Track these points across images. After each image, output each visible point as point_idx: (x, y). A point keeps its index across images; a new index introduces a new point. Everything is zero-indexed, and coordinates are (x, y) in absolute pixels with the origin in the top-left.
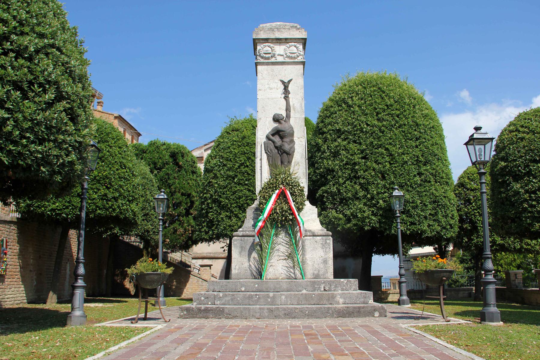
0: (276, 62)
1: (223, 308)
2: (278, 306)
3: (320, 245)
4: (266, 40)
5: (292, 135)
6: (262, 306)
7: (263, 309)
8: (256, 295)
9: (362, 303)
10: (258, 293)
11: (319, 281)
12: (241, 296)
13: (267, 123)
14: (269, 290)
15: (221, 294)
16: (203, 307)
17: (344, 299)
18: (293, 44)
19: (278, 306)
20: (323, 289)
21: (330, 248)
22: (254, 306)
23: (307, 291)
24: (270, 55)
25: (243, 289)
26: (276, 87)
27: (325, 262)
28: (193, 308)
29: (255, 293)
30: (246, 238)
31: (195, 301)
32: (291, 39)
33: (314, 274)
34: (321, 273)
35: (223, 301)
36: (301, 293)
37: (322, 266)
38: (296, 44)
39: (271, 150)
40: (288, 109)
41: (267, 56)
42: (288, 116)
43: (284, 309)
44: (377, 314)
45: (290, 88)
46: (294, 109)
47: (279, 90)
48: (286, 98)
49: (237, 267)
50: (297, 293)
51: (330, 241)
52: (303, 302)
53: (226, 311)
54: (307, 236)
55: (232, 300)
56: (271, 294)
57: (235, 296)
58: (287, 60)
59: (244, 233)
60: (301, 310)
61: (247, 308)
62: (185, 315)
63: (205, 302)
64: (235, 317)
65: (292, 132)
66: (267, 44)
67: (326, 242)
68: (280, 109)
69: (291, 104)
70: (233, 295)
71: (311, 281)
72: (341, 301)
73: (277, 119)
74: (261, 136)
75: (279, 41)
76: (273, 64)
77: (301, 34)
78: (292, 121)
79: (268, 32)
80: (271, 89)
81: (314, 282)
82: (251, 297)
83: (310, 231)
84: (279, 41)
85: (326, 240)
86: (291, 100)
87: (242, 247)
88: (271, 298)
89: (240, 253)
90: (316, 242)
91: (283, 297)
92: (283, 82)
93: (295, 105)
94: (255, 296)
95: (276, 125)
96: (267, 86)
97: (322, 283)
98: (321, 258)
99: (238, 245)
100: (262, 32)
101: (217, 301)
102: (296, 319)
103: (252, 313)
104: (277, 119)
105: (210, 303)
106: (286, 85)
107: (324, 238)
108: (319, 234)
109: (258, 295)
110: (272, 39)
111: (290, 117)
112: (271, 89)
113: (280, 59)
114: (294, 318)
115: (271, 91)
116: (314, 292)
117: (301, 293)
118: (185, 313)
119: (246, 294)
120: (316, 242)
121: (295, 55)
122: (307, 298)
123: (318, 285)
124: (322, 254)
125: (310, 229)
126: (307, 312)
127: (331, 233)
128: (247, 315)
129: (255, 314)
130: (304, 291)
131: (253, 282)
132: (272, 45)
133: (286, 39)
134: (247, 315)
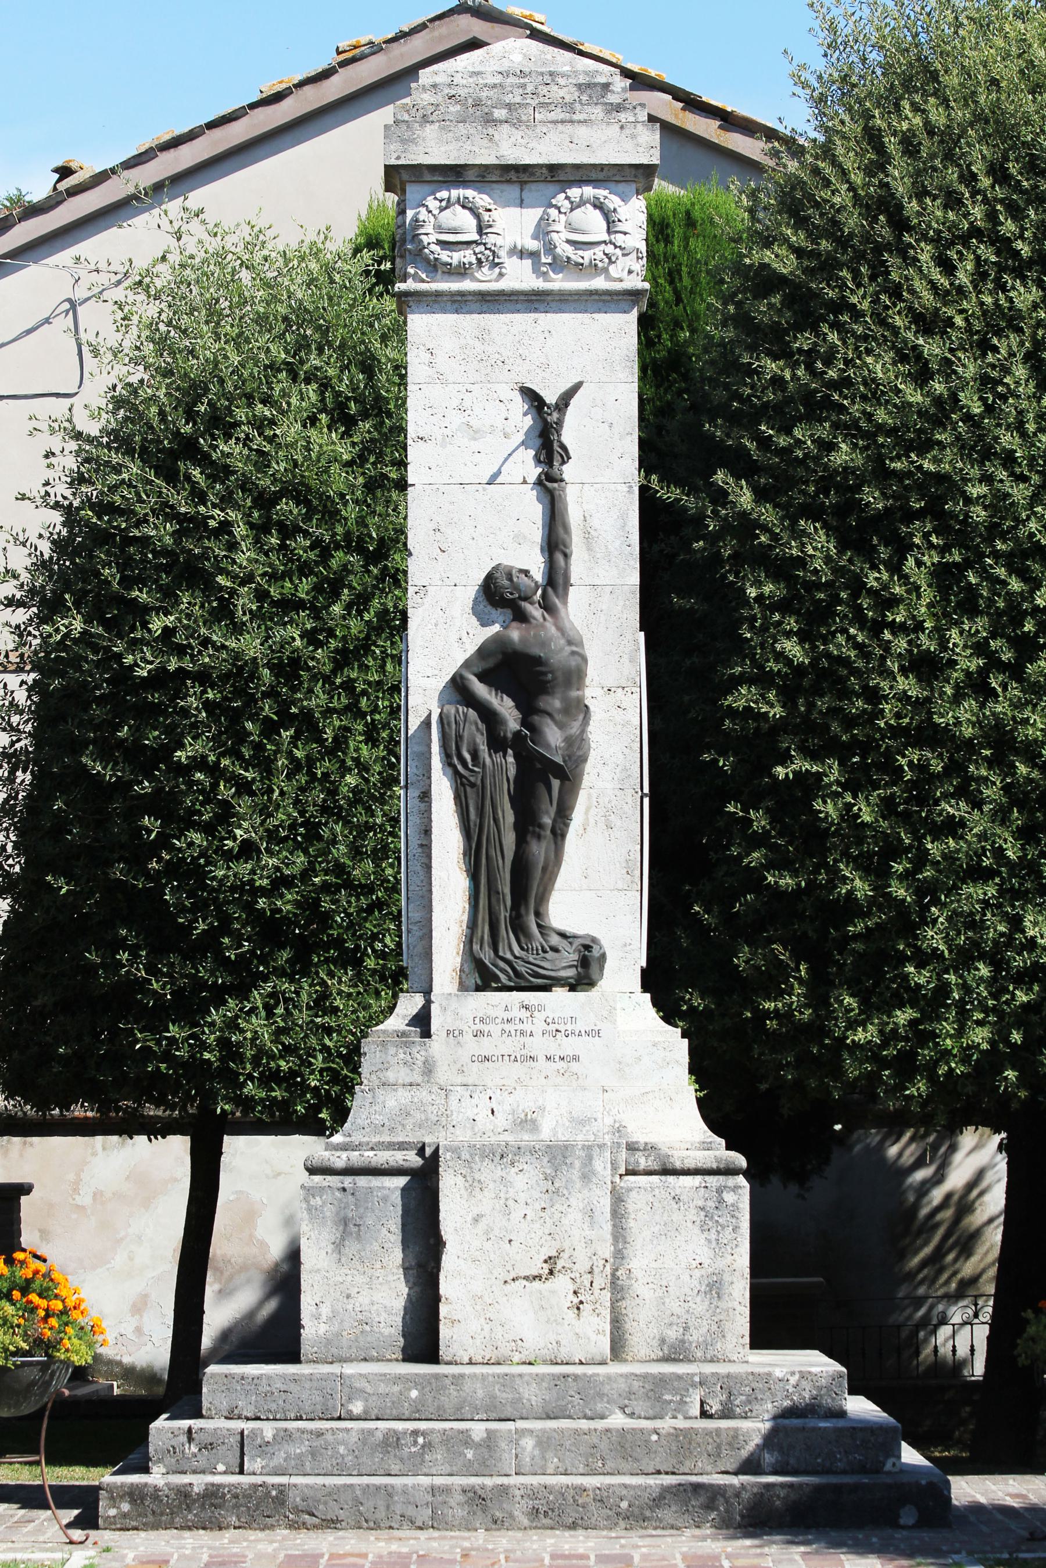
0: (501, 293)
1: (282, 1489)
2: (505, 1480)
3: (692, 1214)
4: (453, 174)
5: (575, 676)
6: (439, 1481)
7: (446, 1490)
8: (415, 1433)
9: (853, 1472)
10: (423, 1425)
11: (679, 1377)
12: (354, 1438)
14: (467, 1412)
15: (268, 1430)
16: (198, 1482)
17: (781, 1450)
18: (589, 191)
19: (505, 1480)
21: (735, 1229)
22: (409, 1481)
23: (632, 1415)
24: (467, 256)
25: (357, 1408)
27: (715, 1288)
28: (156, 1489)
29: (411, 1426)
30: (362, 1181)
31: (159, 1461)
33: (663, 1341)
34: (695, 1336)
35: (279, 1459)
36: (600, 1424)
37: (700, 1305)
38: (602, 193)
39: (475, 755)
40: (555, 544)
42: (556, 580)
43: (532, 1493)
44: (908, 1516)
45: (569, 435)
46: (588, 537)
48: (549, 486)
49: (325, 1310)
50: (584, 1424)
51: (739, 1193)
52: (610, 1465)
53: (295, 1498)
55: (313, 1453)
56: (478, 1430)
57: (329, 1437)
58: (559, 283)
59: (355, 1158)
60: (601, 1498)
61: (378, 1488)
62: (125, 1516)
63: (202, 1462)
64: (332, 1524)
65: (573, 662)
66: (455, 193)
67: (721, 1201)
68: (519, 539)
70: (319, 1434)
71: (645, 1377)
73: (498, 594)
74: (424, 690)
75: (517, 178)
77: (628, 145)
78: (577, 607)
81: (661, 1382)
82: (392, 1442)
83: (650, 1148)
84: (517, 178)
85: (720, 1191)
87: (345, 1222)
88: (477, 1446)
89: (339, 1246)
90: (676, 1199)
91: (528, 1444)
92: (532, 397)
93: (595, 522)
94: (409, 1440)
97: (693, 1385)
98: (697, 1273)
99: (329, 1211)
100: (430, 131)
101: (253, 1458)
102: (580, 1532)
103: (399, 1509)
104: (498, 594)
105: (221, 1468)
107: (713, 1181)
108: (690, 1164)
109: (424, 1434)
110: (486, 168)
111: (567, 584)
113: (519, 276)
114: (573, 1526)
115: (475, 446)
116: (658, 1424)
117: (600, 1424)
118: (126, 1507)
119: (371, 1432)
120: (676, 1199)
122: (626, 1447)
123: (675, 1391)
124: (704, 1254)
125: (651, 1139)
126: (624, 1505)
127: (742, 1161)
128: (381, 1514)
129: (410, 1511)
130: (617, 1420)
131: (398, 1379)
132: (482, 200)
134: (381, 1514)
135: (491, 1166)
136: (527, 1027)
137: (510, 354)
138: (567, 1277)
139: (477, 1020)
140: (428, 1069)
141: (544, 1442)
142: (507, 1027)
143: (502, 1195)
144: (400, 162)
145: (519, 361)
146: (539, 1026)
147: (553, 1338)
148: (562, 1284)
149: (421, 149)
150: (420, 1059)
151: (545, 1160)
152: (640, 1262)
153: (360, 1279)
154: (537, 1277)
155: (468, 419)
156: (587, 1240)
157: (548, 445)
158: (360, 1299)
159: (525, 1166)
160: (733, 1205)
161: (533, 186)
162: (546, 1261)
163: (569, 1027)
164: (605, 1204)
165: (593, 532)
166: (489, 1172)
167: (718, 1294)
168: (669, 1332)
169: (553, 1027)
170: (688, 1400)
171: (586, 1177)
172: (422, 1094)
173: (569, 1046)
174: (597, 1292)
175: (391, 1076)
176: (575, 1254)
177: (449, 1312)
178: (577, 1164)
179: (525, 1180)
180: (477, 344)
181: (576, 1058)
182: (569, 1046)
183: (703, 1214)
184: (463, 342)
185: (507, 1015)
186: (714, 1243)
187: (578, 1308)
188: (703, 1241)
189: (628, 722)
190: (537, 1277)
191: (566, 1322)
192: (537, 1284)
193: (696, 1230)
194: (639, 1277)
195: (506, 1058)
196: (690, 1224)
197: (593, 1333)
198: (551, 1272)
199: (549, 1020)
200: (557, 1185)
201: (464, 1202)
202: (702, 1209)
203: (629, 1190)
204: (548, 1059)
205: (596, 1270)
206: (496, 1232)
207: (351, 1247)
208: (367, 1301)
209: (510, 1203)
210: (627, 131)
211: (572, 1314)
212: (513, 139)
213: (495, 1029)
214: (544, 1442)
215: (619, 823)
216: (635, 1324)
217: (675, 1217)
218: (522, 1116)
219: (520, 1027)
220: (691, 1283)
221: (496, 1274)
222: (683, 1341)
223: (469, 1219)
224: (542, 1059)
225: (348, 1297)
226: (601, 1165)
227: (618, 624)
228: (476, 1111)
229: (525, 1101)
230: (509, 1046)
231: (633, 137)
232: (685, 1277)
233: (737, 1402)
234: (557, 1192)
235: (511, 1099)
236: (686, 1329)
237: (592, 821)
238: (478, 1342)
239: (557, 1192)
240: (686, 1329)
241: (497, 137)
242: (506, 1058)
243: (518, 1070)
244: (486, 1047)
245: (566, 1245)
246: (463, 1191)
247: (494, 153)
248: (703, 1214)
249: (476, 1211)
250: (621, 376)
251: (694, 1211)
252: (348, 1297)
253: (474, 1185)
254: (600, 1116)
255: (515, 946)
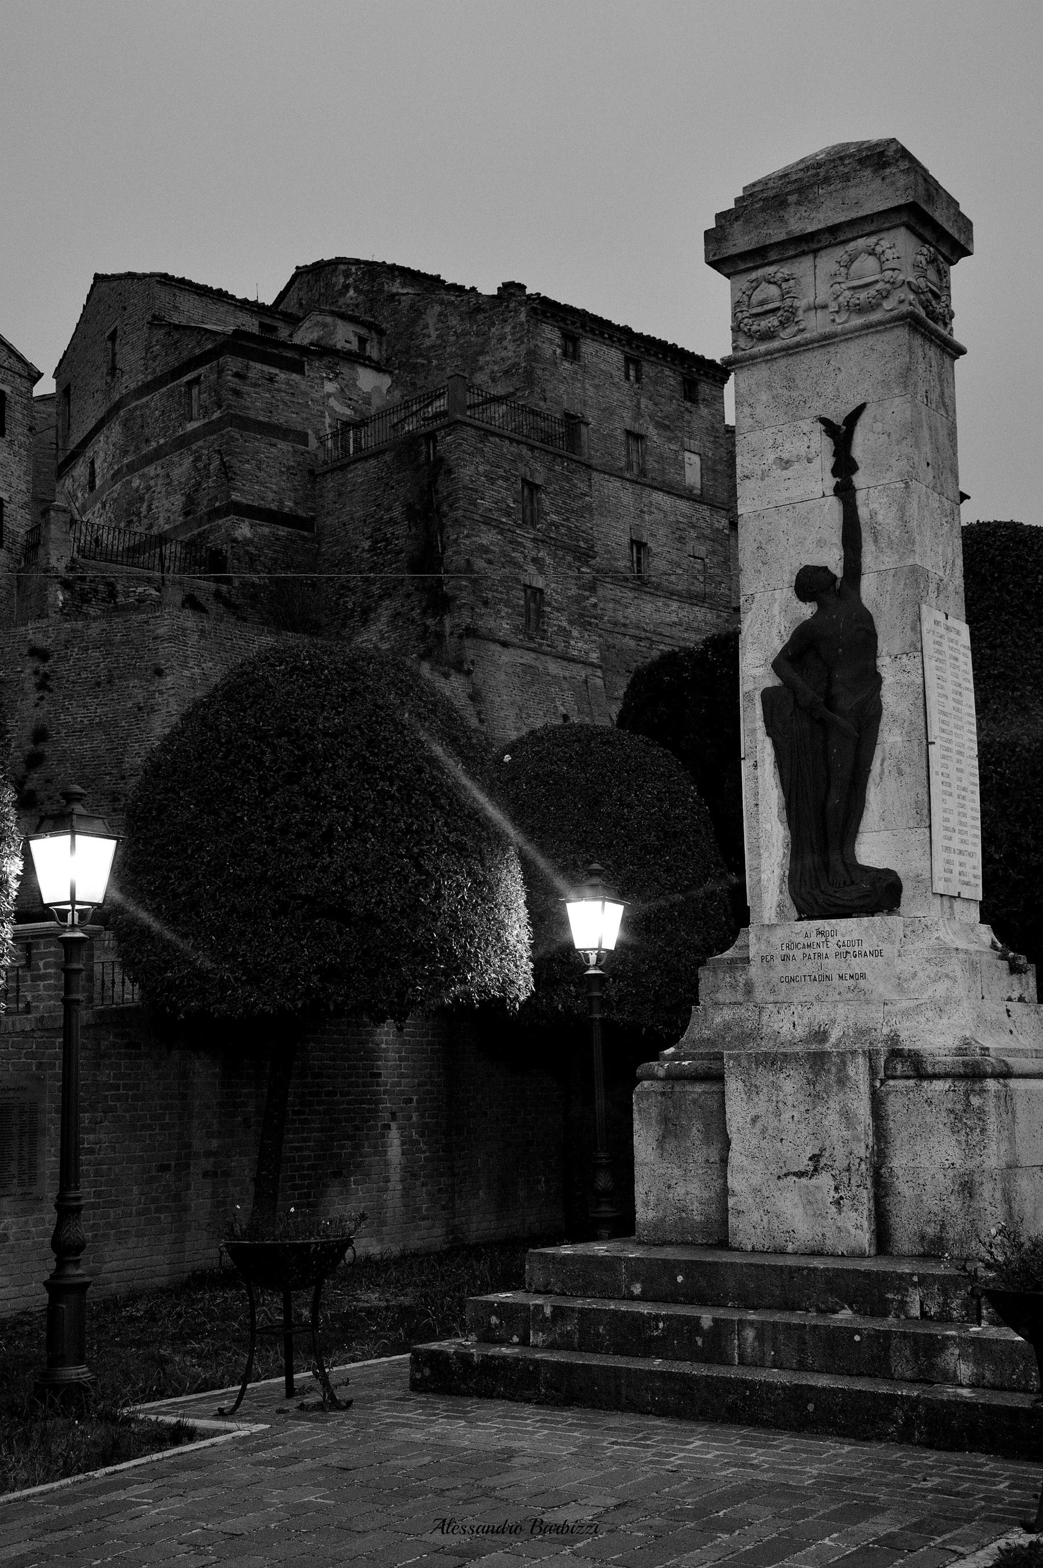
13: (776, 610)
18: (861, 243)
20: (915, 1312)
24: (773, 321)
26: (803, 451)
32: (852, 223)
33: (923, 1237)
34: (951, 1234)
37: (955, 1205)
41: (764, 324)
45: (858, 452)
47: (817, 462)
48: (845, 492)
54: (894, 1078)
60: (798, 1394)
67: (968, 1104)
68: (821, 543)
69: (863, 512)
72: (965, 1371)
73: (810, 583)
74: (755, 671)
75: (807, 244)
76: (789, 351)
78: (869, 588)
79: (761, 218)
80: (785, 464)
86: (860, 496)
89: (661, 1143)
90: (929, 1102)
92: (829, 427)
93: (880, 518)
95: (807, 610)
96: (771, 456)
97: (915, 1285)
98: (951, 1173)
99: (654, 1112)
104: (810, 583)
106: (841, 434)
110: (781, 245)
112: (785, 464)
113: (816, 324)
115: (788, 473)
118: (427, 1372)
120: (929, 1102)
121: (872, 291)
133: (833, 230)
135: (765, 1072)
136: (823, 950)
137: (810, 394)
138: (829, 1174)
139: (784, 946)
140: (749, 989)
141: (761, 1329)
142: (807, 951)
143: (774, 1098)
144: (716, 258)
145: (816, 398)
146: (833, 948)
147: (819, 1230)
148: (825, 1180)
149: (731, 243)
150: (741, 981)
151: (808, 1066)
152: (899, 1161)
153: (677, 1172)
154: (800, 1174)
155: (780, 453)
156: (848, 1138)
157: (844, 466)
158: (678, 1189)
159: (792, 1072)
160: (979, 1108)
161: (823, 253)
162: (810, 1159)
163: (856, 949)
164: (862, 1108)
165: (878, 528)
166: (763, 1077)
167: (970, 1193)
168: (929, 1230)
169: (843, 949)
170: (908, 1299)
171: (842, 1081)
172: (742, 1012)
173: (857, 965)
174: (854, 1188)
175: (720, 997)
176: (835, 1152)
177: (735, 1204)
178: (834, 1069)
179: (791, 1084)
180: (785, 391)
181: (863, 976)
182: (857, 965)
183: (952, 1116)
184: (775, 392)
185: (806, 941)
186: (964, 1143)
187: (839, 1203)
188: (954, 1142)
189: (913, 683)
190: (800, 1174)
191: (830, 1217)
192: (804, 1180)
193: (947, 1131)
194: (900, 1174)
195: (808, 978)
196: (941, 1126)
197: (855, 1229)
198: (816, 1170)
199: (840, 944)
200: (818, 1089)
201: (744, 1104)
202: (952, 1111)
203: (888, 1093)
204: (841, 977)
205: (853, 1168)
206: (770, 1131)
207: (670, 1145)
208: (683, 1191)
209: (780, 1105)
210: (887, 181)
211: (833, 1209)
212: (798, 215)
213: (798, 953)
214: (761, 1329)
215: (908, 770)
216: (898, 1219)
217: (928, 1119)
218: (817, 1028)
219: (818, 950)
220: (945, 1182)
221: (771, 1170)
222: (941, 1239)
223: (748, 1119)
224: (835, 977)
225: (669, 1187)
226: (858, 1071)
227: (899, 601)
228: (781, 1024)
229: (820, 1014)
230: (809, 968)
231: (893, 183)
232: (940, 1176)
233: (953, 1305)
234: (818, 1096)
235: (809, 1014)
236: (943, 1226)
237: (886, 771)
238: (758, 1231)
239: (818, 1096)
240: (943, 1226)
241: (786, 217)
242: (808, 978)
243: (815, 989)
244: (792, 969)
245: (827, 1143)
246: (743, 1096)
247: (784, 231)
248: (952, 1116)
249: (753, 1113)
250: (896, 391)
251: (944, 1114)
252: (669, 1187)
253: (752, 1090)
254: (879, 1026)
255: (837, 884)
